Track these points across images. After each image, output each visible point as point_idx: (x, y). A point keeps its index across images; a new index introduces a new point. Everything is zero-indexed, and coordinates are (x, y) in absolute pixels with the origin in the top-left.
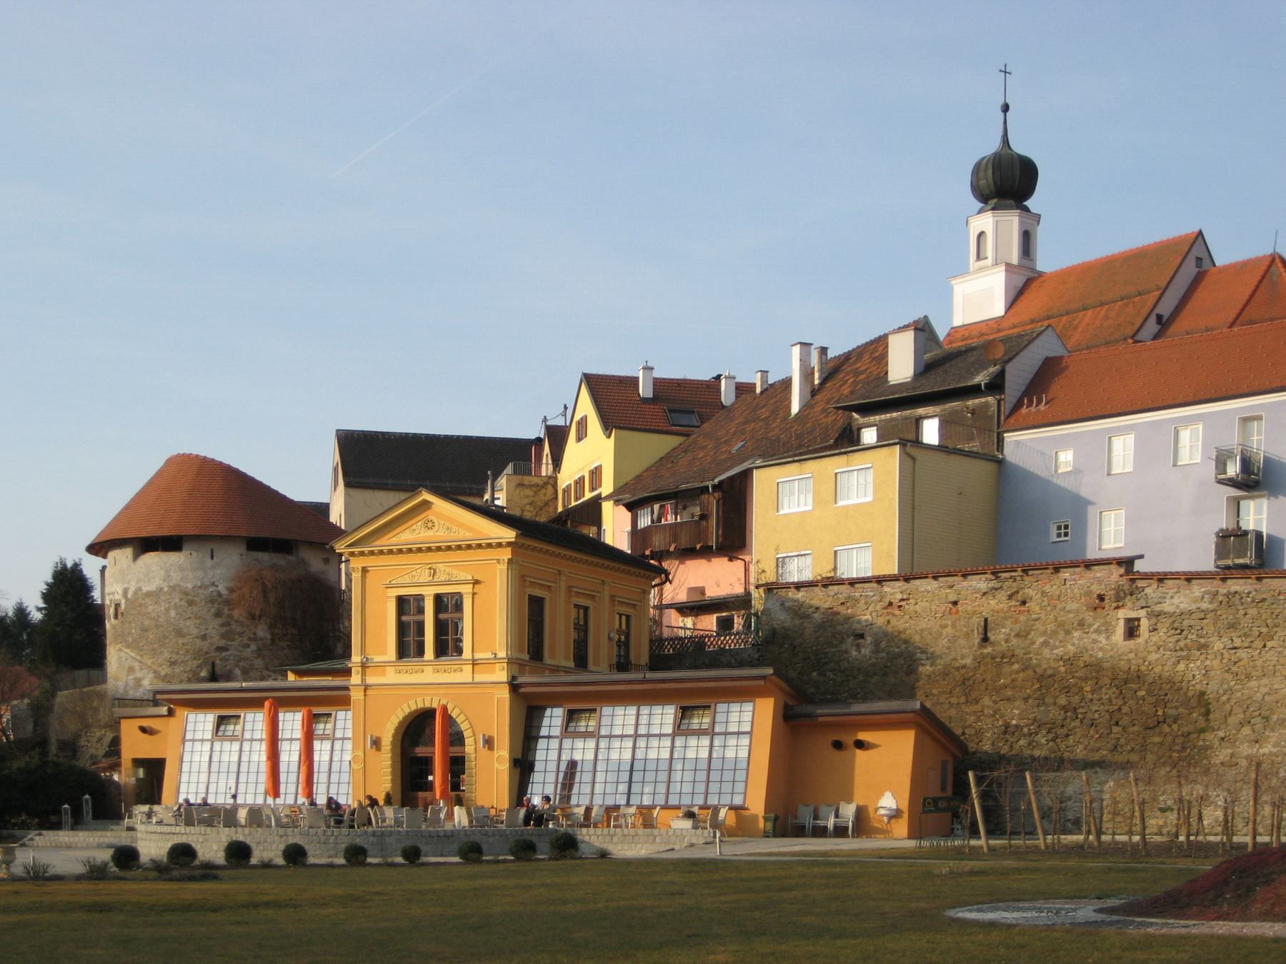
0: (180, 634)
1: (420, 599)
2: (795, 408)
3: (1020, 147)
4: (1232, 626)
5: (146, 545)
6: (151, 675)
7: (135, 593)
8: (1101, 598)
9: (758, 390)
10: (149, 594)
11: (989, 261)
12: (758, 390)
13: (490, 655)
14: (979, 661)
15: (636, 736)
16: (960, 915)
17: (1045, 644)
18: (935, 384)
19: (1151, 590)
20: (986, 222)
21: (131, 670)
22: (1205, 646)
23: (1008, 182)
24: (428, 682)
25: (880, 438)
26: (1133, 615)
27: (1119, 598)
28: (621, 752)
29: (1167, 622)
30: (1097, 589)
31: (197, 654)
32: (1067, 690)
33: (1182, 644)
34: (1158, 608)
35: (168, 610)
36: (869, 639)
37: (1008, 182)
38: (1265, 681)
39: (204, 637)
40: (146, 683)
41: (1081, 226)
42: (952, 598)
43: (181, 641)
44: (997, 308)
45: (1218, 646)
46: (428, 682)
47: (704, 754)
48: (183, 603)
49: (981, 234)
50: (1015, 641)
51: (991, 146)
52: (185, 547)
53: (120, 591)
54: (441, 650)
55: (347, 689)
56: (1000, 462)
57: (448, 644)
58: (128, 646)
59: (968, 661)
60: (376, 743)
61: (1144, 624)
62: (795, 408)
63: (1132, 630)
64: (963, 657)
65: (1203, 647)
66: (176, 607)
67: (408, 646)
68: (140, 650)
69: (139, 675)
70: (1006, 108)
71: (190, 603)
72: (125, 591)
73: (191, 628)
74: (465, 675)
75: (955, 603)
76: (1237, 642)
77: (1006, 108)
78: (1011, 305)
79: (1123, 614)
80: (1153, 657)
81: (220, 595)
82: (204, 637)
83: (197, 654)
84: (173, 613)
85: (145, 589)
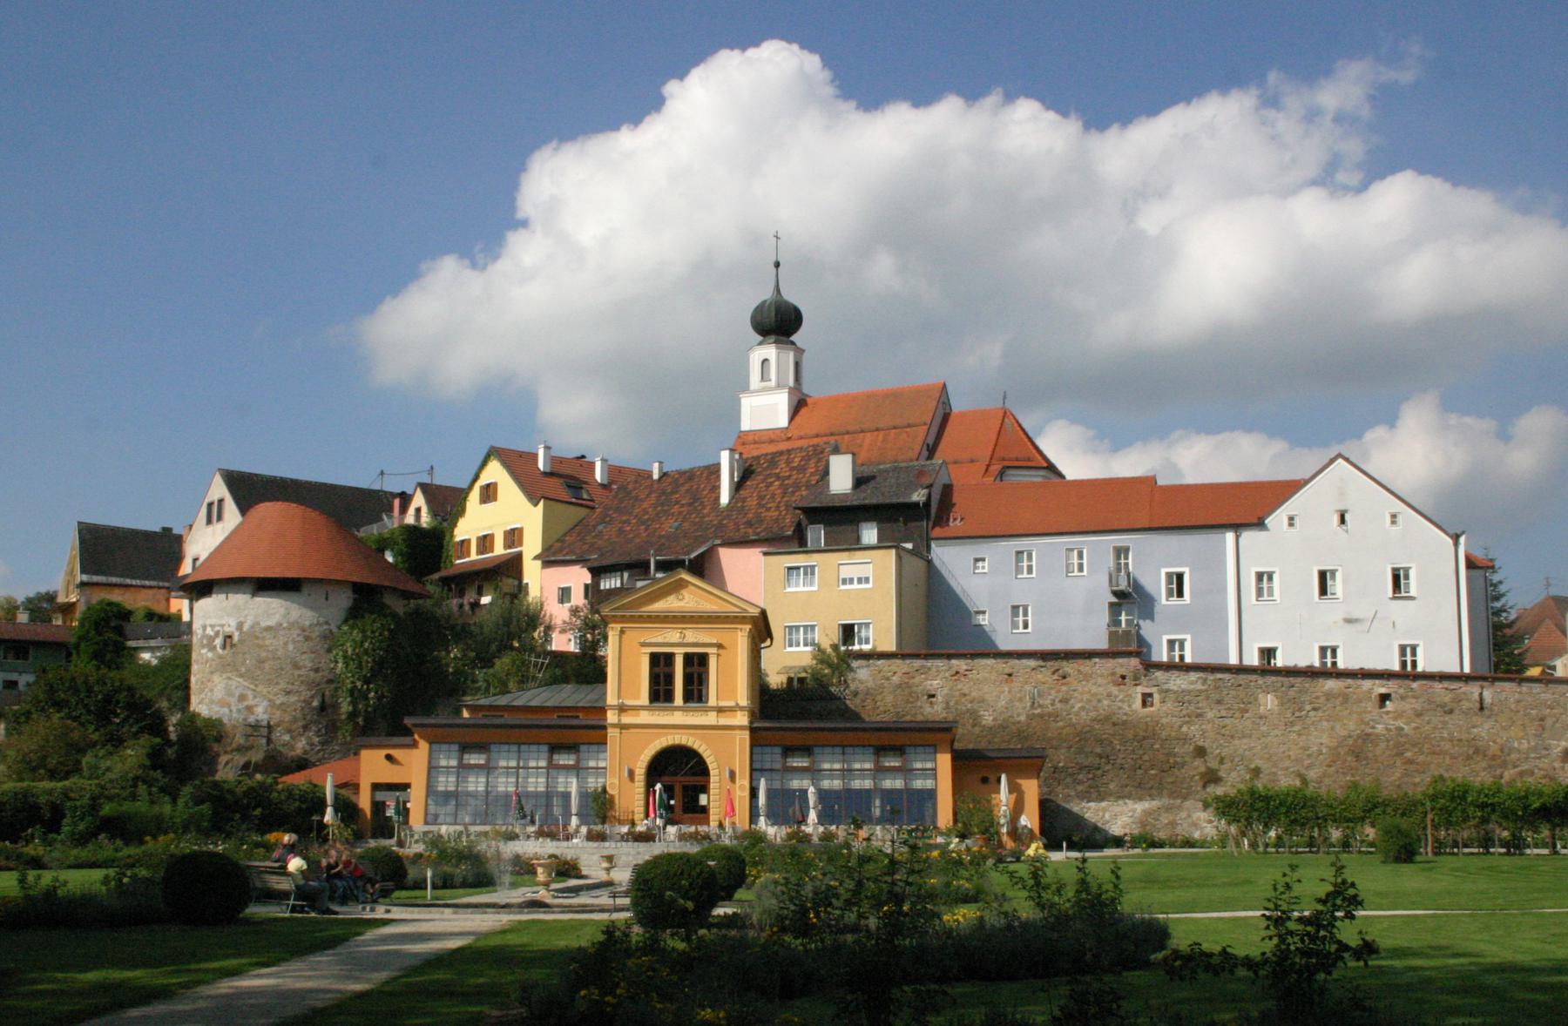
0: (296, 666)
1: (669, 658)
2: (725, 498)
3: (791, 296)
4: (1219, 702)
5: (263, 586)
6: (265, 703)
7: (252, 627)
8: (1123, 677)
9: (656, 477)
10: (268, 629)
11: (773, 383)
12: (656, 477)
13: (732, 704)
14: (1031, 717)
16: (180, 1007)
17: (1083, 708)
18: (869, 497)
20: (770, 351)
21: (242, 698)
22: (1199, 715)
23: (779, 323)
24: (678, 724)
25: (880, 539)
26: (1148, 690)
27: (1136, 680)
31: (311, 685)
32: (1101, 742)
35: (286, 644)
39: (317, 670)
40: (260, 710)
42: (1008, 671)
43: (297, 673)
45: (1210, 715)
46: (678, 724)
49: (765, 361)
50: (1059, 706)
51: (767, 294)
53: (233, 623)
54: (688, 697)
56: (929, 562)
57: (696, 691)
58: (241, 676)
59: (1023, 718)
60: (631, 774)
61: (1156, 697)
62: (725, 498)
63: (1146, 699)
65: (1199, 715)
66: (294, 642)
67: (660, 692)
68: (253, 679)
69: (250, 702)
70: (777, 265)
71: (307, 638)
72: (240, 626)
73: (306, 661)
74: (711, 719)
76: (1224, 713)
77: (777, 265)
78: (792, 419)
79: (1140, 689)
80: (1164, 721)
82: (317, 670)
83: (311, 685)
84: (291, 647)
85: (263, 624)
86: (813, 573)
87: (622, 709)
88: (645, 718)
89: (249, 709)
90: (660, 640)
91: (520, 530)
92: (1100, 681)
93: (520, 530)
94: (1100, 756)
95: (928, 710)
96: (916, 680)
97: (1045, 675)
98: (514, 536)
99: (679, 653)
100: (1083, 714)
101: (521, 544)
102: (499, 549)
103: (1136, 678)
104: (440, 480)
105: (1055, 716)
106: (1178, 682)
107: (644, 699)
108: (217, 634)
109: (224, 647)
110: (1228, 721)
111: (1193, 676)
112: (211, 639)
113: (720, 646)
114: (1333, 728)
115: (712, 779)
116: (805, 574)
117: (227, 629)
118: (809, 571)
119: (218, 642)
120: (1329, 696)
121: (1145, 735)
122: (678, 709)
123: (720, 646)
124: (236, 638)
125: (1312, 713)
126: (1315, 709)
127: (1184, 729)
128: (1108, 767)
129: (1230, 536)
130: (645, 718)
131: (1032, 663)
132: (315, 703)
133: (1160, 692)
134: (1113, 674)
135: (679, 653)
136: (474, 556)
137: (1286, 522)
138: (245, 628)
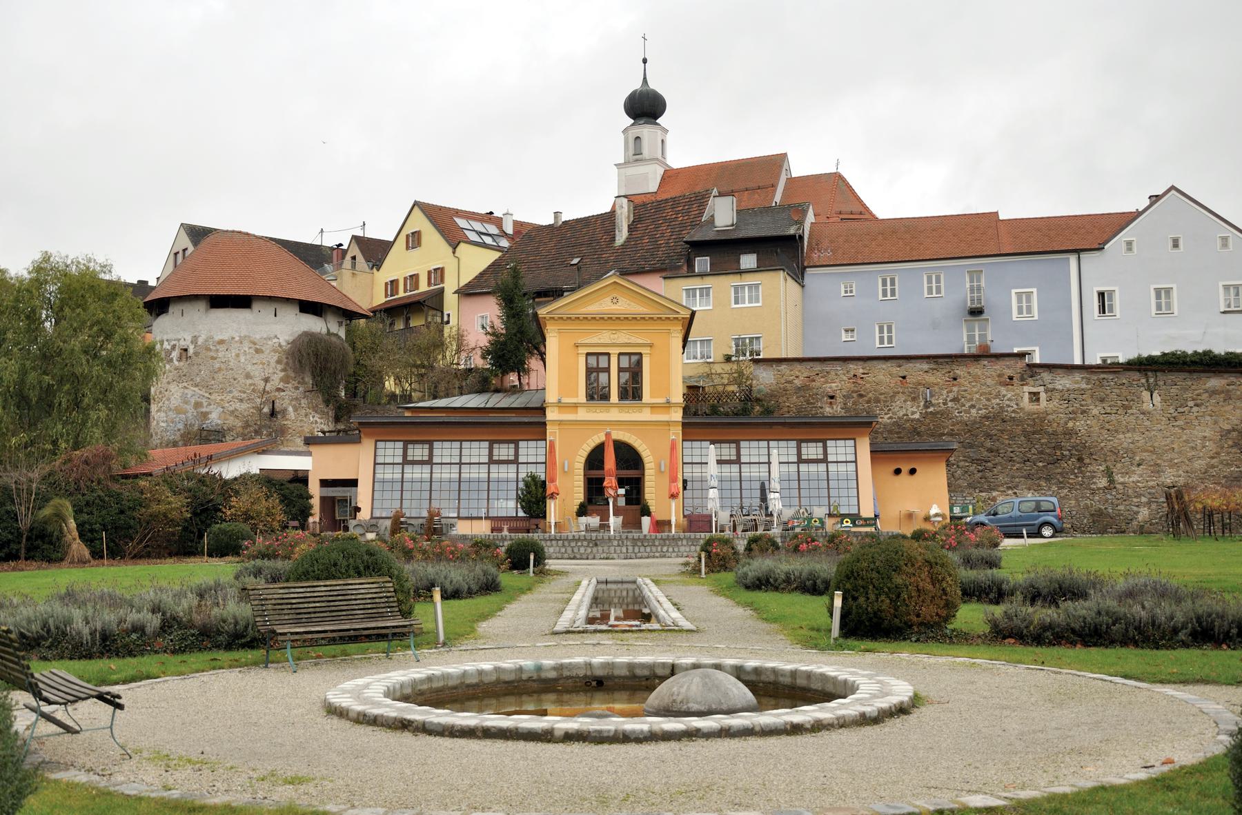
3: (653, 85)
4: (1102, 400)
8: (1011, 378)
14: (925, 416)
15: (460, 464)
19: (1046, 376)
24: (616, 421)
26: (1035, 390)
28: (445, 474)
29: (1057, 395)
30: (1009, 372)
33: (1071, 409)
34: (1050, 386)
36: (839, 400)
37: (645, 107)
38: (1129, 435)
41: (688, 143)
44: (653, 186)
45: (1095, 411)
47: (427, 476)
48: (252, 351)
50: (950, 404)
51: (637, 85)
52: (171, 309)
53: (189, 338)
55: (545, 424)
57: (631, 392)
58: (197, 386)
61: (1043, 396)
63: (1035, 397)
64: (913, 413)
65: (1083, 412)
70: (645, 61)
72: (195, 340)
74: (646, 415)
75: (904, 377)
77: (645, 61)
79: (1026, 389)
80: (1050, 417)
81: (280, 346)
85: (217, 338)
86: (708, 295)
87: (560, 405)
88: (583, 415)
89: (205, 415)
90: (595, 340)
91: (442, 270)
92: (989, 381)
93: (442, 270)
94: (990, 450)
95: (828, 410)
96: (817, 384)
97: (938, 377)
98: (439, 273)
99: (614, 351)
100: (973, 411)
101: (442, 281)
102: (423, 287)
103: (1022, 379)
104: (371, 233)
105: (945, 414)
106: (1064, 382)
107: (582, 398)
108: (174, 347)
109: (180, 359)
110: (1113, 417)
111: (1078, 376)
112: (169, 353)
113: (651, 346)
114: (1216, 423)
115: (647, 472)
116: (701, 295)
117: (183, 344)
118: (705, 292)
119: (175, 355)
120: (1213, 393)
121: (1035, 428)
122: (615, 405)
123: (651, 346)
124: (191, 351)
125: (1195, 409)
126: (1196, 405)
127: (1070, 424)
128: (998, 460)
129: (1073, 259)
130: (583, 415)
131: (925, 366)
132: (266, 410)
133: (1046, 391)
134: (1000, 376)
135: (614, 351)
136: (401, 294)
137: (1124, 246)
138: (200, 341)
